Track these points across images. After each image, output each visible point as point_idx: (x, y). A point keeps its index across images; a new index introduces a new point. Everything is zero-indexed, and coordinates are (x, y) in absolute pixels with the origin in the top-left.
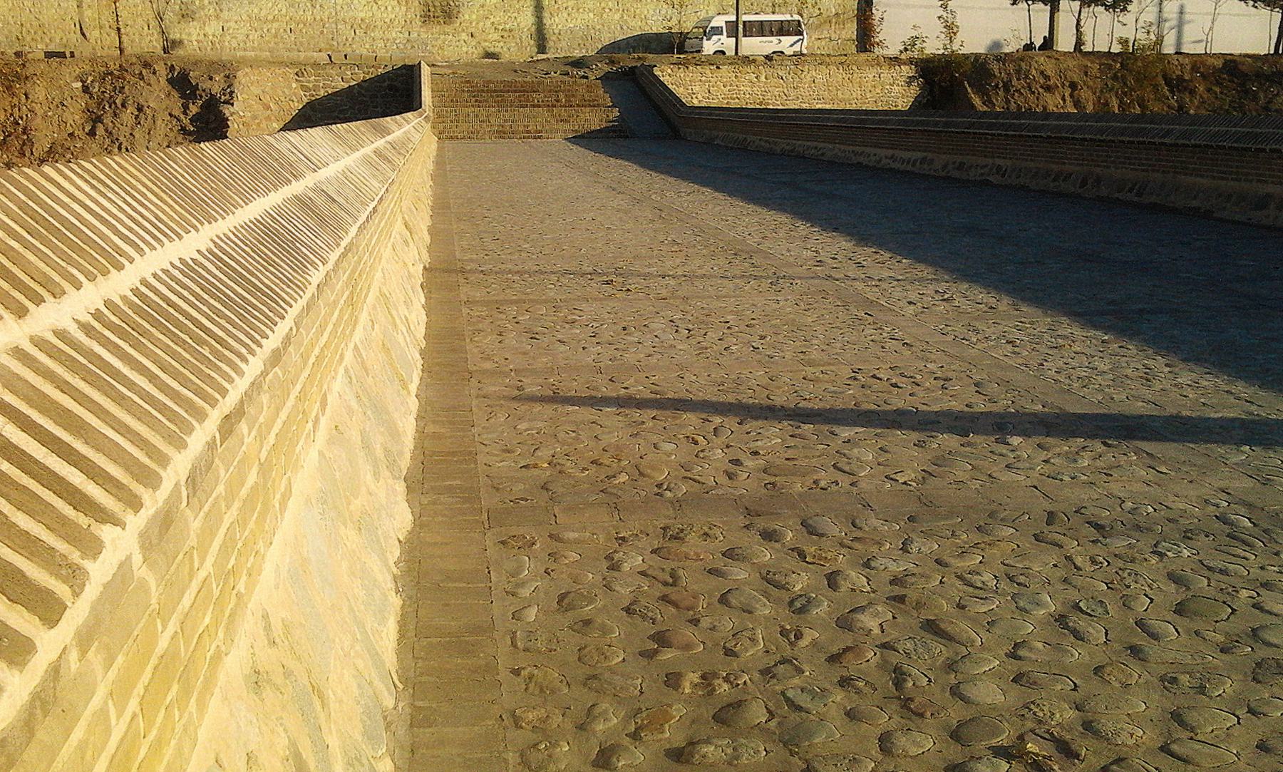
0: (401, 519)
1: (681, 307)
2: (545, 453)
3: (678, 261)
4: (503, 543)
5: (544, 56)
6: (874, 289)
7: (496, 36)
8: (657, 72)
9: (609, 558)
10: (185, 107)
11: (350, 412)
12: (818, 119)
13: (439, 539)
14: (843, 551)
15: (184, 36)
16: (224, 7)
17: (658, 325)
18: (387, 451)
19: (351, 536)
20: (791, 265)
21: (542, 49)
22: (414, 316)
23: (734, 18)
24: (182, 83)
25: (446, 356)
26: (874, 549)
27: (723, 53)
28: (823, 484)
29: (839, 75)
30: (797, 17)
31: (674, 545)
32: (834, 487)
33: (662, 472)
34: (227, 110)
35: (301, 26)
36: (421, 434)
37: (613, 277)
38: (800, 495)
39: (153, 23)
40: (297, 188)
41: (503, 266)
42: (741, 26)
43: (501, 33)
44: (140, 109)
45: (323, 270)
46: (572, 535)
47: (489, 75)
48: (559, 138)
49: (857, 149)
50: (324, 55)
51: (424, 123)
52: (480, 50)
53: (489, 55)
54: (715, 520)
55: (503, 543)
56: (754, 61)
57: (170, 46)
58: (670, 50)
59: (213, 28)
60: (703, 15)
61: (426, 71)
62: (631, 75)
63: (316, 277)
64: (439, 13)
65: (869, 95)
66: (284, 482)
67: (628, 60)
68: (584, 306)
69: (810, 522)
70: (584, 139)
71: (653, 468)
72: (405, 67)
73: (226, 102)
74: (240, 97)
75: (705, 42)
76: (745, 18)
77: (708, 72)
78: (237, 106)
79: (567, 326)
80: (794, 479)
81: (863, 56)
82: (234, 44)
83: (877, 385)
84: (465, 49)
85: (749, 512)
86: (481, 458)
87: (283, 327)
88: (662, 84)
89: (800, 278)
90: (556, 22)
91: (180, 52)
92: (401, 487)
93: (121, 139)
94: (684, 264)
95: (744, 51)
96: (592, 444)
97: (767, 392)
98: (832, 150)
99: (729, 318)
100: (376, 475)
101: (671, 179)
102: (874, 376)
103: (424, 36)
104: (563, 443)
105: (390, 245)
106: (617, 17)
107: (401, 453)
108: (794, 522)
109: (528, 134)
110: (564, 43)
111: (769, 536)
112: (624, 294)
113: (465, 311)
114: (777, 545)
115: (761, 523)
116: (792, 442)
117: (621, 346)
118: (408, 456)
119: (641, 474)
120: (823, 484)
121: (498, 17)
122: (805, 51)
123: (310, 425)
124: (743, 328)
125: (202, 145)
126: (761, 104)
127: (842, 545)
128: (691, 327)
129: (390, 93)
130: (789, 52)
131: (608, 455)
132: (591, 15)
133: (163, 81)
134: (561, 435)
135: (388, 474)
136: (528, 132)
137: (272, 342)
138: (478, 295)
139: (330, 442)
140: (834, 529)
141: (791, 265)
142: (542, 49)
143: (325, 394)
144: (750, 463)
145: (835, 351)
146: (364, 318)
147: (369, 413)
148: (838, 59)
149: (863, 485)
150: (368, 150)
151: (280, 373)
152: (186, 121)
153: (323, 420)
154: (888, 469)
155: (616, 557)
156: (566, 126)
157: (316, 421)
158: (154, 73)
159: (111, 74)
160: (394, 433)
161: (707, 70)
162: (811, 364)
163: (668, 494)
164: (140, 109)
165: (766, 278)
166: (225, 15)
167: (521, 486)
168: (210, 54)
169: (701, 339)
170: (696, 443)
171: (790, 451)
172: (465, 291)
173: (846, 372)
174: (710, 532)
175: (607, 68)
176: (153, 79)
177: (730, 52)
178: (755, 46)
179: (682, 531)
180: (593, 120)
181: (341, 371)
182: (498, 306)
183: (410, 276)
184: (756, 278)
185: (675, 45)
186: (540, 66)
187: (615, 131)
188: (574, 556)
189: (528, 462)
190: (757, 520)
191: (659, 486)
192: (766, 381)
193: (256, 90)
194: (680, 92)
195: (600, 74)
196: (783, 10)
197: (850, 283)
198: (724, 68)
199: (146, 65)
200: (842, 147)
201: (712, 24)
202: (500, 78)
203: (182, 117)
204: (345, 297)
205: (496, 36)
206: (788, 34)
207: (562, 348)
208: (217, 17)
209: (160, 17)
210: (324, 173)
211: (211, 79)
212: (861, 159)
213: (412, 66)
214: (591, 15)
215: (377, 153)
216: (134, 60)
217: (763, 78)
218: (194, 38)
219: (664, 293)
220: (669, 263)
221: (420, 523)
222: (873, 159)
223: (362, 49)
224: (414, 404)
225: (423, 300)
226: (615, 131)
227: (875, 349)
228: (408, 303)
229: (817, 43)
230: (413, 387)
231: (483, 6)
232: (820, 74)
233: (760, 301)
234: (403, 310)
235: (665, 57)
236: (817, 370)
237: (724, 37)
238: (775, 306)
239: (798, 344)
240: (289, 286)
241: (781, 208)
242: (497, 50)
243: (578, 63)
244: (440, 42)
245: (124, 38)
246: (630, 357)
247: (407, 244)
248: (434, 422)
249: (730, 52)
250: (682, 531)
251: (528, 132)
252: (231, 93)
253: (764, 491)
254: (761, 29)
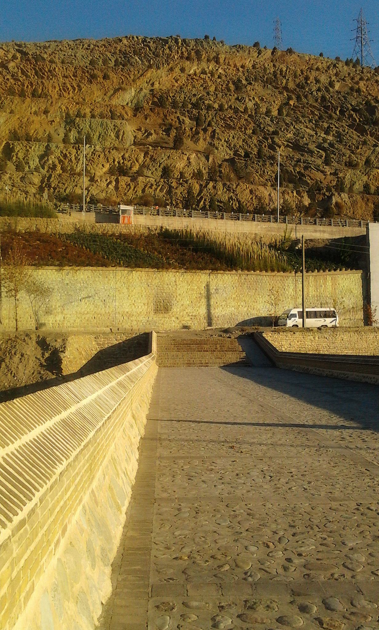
0: (105, 589)
1: (268, 463)
2: (187, 550)
3: (269, 436)
4: (157, 607)
5: (210, 328)
6: (371, 455)
7: (188, 318)
8: (264, 335)
9: (213, 619)
10: (43, 354)
11: (82, 531)
12: (343, 360)
13: (123, 603)
14: (345, 621)
15: (46, 322)
16: (65, 308)
17: (255, 473)
18: (103, 550)
19: (71, 607)
20: (328, 440)
21: (210, 324)
22: (131, 466)
23: (301, 310)
24: (43, 344)
25: (145, 491)
26: (362, 621)
27: (297, 326)
28: (336, 576)
29: (355, 337)
30: (332, 309)
31: (249, 612)
32: (342, 579)
33: (248, 564)
34: (62, 355)
35: (99, 316)
36: (124, 535)
37: (234, 444)
38: (323, 583)
39: (33, 316)
40: (64, 415)
41: (180, 437)
42: (305, 314)
43: (190, 317)
44: (22, 355)
45: (65, 463)
46: (194, 604)
47: (184, 336)
48: (216, 367)
49: (364, 375)
50: (108, 329)
51: (151, 361)
52: (181, 325)
53: (185, 327)
54: (274, 597)
55: (157, 607)
56: (312, 330)
57: (39, 325)
58: (270, 325)
59: (59, 318)
60: (286, 308)
61: (154, 335)
62: (251, 336)
63: (60, 468)
64: (162, 308)
65: (371, 346)
66: (30, 584)
67: (250, 330)
68: (218, 461)
69: (327, 601)
70: (229, 367)
71: (243, 562)
72: (145, 333)
73: (61, 352)
74: (68, 349)
75: (288, 321)
76: (307, 310)
77: (289, 335)
78: (67, 353)
79: (208, 473)
80: (318, 572)
81: (367, 328)
82: (69, 325)
83: (370, 513)
84: (174, 324)
85: (294, 593)
86: (153, 552)
87: (30, 505)
88: (267, 341)
89: (332, 447)
90: (216, 312)
91: (44, 329)
92: (108, 570)
93: (13, 369)
94: (271, 437)
95: (306, 326)
96: (213, 545)
97: (309, 516)
98: (353, 375)
99: (293, 470)
100: (93, 566)
101: (269, 389)
102: (368, 508)
103: (155, 319)
104: (198, 544)
105: (122, 429)
106: (245, 309)
107: (111, 550)
108: (318, 600)
109: (201, 365)
110: (220, 322)
111: (304, 609)
112: (238, 454)
113: (158, 462)
114: (308, 616)
115: (300, 600)
116: (321, 548)
117: (234, 485)
118: (115, 550)
119: (237, 566)
120: (336, 576)
121: (189, 310)
122: (338, 325)
123: (53, 546)
124: (300, 476)
125: (15, 401)
126: (316, 350)
127: (344, 617)
128: (272, 475)
129: (137, 346)
130: (330, 325)
131: (220, 552)
132: (233, 309)
133: (34, 342)
134: (197, 540)
135: (101, 563)
136: (202, 363)
137: (22, 515)
138: (166, 453)
139: (66, 552)
140: (340, 606)
141: (327, 440)
142: (210, 324)
143: (66, 526)
144: (297, 561)
145: (348, 492)
146: (99, 474)
147: (94, 529)
148: (355, 329)
149: (359, 577)
150: (114, 383)
151: (28, 528)
152: (43, 361)
153: (63, 542)
154: (373, 567)
155: (218, 619)
156: (220, 361)
157: (58, 541)
158: (30, 339)
159: (11, 339)
160: (108, 539)
161: (289, 334)
162: (334, 499)
163: (250, 579)
164: (22, 355)
165: (315, 447)
166: (66, 312)
167: (172, 571)
168: (57, 329)
169: (277, 482)
170: (268, 547)
171: (320, 554)
172: (161, 451)
173: (353, 505)
174: (271, 605)
175: (240, 333)
176: (29, 341)
177: (300, 326)
178: (312, 322)
179: (255, 603)
180: (233, 358)
181: (80, 508)
182: (175, 460)
183: (131, 444)
184: (309, 446)
185: (274, 322)
186: (208, 332)
187: (243, 363)
188: (194, 617)
189: (178, 555)
190: (297, 598)
191: (246, 573)
192: (309, 509)
193: (76, 346)
194: (275, 344)
195: (237, 336)
196: (326, 306)
197: (358, 451)
198: (297, 333)
199: (27, 335)
200: (357, 374)
201: (291, 313)
202: (189, 338)
203: (41, 359)
204: (85, 468)
205: (188, 318)
206: (329, 317)
207: (204, 486)
208: (62, 313)
209: (36, 314)
210: (84, 402)
211: (56, 341)
212: (367, 380)
213: (148, 333)
214: (233, 309)
215: (120, 384)
216: (22, 333)
217: (317, 338)
218: (51, 322)
219: (260, 454)
220: (264, 437)
221: (115, 594)
222: (373, 380)
223: (127, 326)
224: (123, 518)
225: (137, 456)
226: (243, 363)
227: (370, 491)
228: (128, 460)
229: (344, 321)
230: (124, 509)
231: (182, 305)
232: (346, 337)
233: (310, 460)
234: (124, 465)
235: (268, 328)
236: (337, 503)
237: (297, 319)
238: (317, 464)
239: (328, 487)
240: (41, 478)
241: (324, 407)
242: (189, 325)
243: (226, 331)
244: (162, 322)
245: (19, 323)
246: (238, 493)
247: (132, 426)
248: (133, 529)
249: (300, 326)
250: (255, 603)
251: (202, 363)
252: (65, 347)
253: (303, 580)
254: (315, 315)
